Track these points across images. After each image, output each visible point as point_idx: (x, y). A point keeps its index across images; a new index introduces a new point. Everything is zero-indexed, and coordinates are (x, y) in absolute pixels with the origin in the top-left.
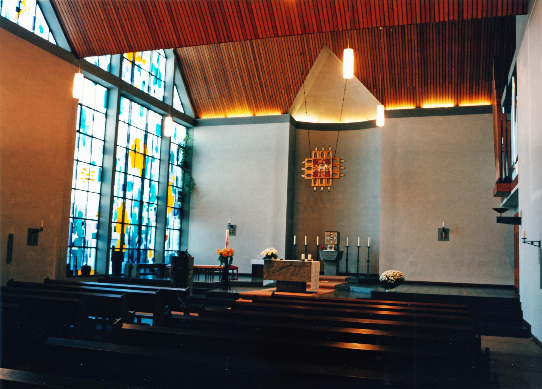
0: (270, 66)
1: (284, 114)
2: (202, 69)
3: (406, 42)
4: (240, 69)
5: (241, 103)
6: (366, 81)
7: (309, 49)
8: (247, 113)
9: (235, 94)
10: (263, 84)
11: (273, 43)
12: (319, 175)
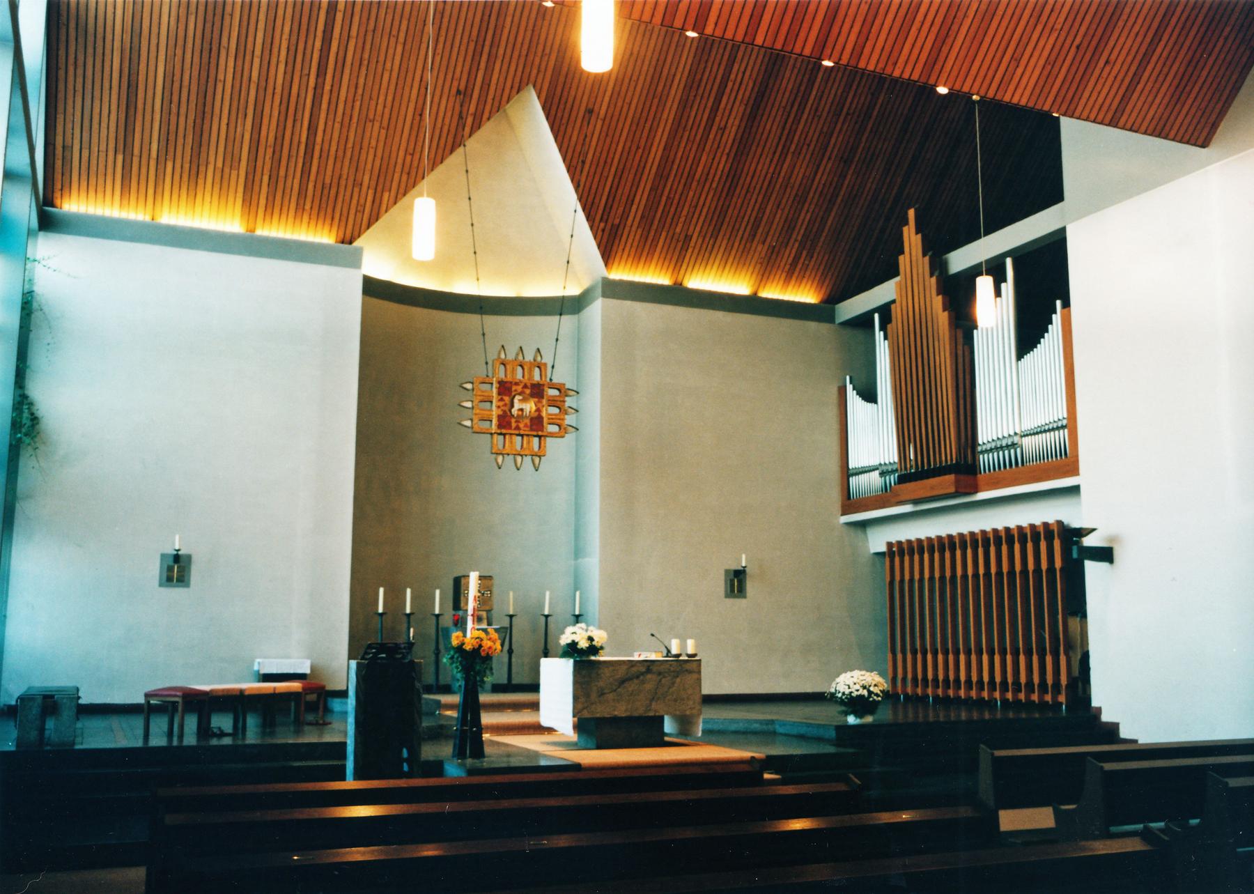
0: (358, 104)
1: (343, 242)
2: (132, 55)
3: (715, 128)
4: (263, 87)
5: (222, 184)
6: (590, 200)
7: (486, 85)
8: (231, 222)
9: (215, 158)
10: (317, 148)
11: (393, 40)
12: (514, 425)
